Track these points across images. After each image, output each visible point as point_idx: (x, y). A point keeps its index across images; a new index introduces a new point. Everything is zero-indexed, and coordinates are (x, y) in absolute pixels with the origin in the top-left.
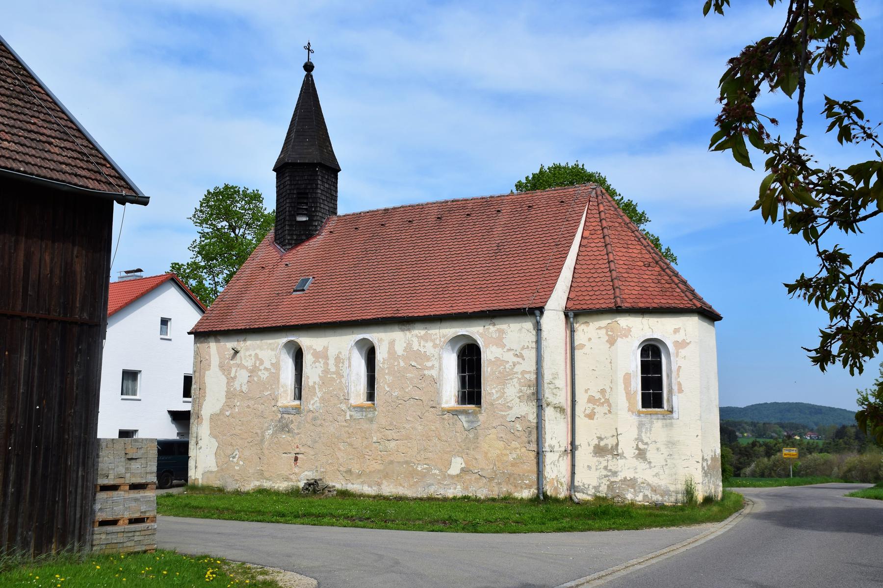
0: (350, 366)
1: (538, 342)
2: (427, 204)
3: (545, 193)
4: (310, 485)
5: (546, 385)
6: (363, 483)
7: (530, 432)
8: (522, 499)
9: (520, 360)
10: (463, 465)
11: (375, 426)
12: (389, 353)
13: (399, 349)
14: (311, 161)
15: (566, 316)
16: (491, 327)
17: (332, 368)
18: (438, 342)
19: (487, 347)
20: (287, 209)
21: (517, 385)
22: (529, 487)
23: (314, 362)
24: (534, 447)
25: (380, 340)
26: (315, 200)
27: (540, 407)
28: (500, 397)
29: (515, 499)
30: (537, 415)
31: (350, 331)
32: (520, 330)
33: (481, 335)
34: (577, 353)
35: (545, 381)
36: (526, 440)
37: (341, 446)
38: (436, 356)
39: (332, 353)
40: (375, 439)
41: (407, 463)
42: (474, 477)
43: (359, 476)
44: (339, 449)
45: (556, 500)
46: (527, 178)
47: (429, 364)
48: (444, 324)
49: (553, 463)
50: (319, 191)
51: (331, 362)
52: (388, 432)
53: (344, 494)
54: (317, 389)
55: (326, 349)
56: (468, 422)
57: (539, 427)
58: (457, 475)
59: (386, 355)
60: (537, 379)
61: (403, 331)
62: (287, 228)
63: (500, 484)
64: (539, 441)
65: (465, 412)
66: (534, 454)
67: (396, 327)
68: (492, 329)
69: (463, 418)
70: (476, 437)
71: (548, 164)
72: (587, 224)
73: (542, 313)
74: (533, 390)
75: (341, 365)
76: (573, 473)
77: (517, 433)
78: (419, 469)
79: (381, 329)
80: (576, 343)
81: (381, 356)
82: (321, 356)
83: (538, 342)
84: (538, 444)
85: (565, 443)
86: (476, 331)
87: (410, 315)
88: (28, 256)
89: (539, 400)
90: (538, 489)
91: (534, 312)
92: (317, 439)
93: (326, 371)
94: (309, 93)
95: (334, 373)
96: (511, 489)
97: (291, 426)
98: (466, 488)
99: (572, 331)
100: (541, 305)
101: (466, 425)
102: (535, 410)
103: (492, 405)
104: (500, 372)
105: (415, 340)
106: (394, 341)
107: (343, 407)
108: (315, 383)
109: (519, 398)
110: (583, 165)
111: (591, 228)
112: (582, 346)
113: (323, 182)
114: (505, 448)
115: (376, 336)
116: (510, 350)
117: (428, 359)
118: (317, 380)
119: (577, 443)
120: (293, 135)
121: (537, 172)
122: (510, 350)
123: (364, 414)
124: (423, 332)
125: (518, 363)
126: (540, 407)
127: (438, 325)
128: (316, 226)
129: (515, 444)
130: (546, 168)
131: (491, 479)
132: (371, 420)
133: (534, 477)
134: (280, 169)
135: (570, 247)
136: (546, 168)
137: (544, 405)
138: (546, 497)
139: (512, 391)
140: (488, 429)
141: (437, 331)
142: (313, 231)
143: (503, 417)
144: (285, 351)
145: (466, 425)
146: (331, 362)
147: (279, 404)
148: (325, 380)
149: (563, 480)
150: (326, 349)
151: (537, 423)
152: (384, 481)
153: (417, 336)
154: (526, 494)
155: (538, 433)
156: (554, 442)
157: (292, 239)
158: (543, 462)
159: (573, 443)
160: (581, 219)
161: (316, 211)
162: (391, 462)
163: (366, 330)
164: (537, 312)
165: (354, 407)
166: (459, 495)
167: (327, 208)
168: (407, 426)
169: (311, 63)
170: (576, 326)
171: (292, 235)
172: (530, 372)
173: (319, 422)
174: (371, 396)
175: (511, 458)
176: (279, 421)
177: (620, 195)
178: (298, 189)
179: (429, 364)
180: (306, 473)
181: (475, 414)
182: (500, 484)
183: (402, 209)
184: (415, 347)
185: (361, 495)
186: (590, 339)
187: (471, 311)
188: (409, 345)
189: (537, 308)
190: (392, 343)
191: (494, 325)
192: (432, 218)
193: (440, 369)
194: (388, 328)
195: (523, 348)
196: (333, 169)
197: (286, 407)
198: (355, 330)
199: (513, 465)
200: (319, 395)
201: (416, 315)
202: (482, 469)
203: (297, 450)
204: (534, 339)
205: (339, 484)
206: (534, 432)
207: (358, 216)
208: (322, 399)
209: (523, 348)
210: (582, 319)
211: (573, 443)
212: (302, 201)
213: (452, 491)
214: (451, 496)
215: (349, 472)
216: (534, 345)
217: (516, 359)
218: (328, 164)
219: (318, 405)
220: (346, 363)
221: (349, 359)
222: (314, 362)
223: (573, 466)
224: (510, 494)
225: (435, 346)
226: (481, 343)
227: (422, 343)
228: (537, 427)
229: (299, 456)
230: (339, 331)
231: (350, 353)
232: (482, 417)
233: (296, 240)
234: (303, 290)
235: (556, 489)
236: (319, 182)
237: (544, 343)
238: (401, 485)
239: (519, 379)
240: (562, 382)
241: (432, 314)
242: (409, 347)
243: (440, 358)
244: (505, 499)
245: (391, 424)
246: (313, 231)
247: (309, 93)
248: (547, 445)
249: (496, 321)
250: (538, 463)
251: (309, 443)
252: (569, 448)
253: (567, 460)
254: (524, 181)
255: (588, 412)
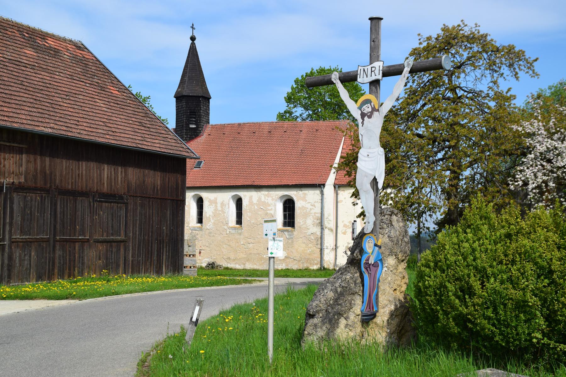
0: (229, 208)
1: (322, 200)
2: (262, 123)
3: (324, 123)
4: (210, 265)
5: (325, 219)
6: (236, 264)
7: (318, 240)
8: (313, 270)
9: (313, 207)
10: (286, 255)
11: (242, 237)
12: (249, 202)
13: (255, 200)
14: (197, 95)
15: (335, 187)
16: (300, 192)
17: (219, 208)
18: (274, 198)
19: (298, 201)
20: (185, 121)
21: (312, 219)
22: (317, 264)
23: (210, 205)
24: (319, 246)
25: (245, 196)
26: (200, 116)
27: (322, 229)
28: (304, 224)
29: (310, 269)
30: (321, 232)
31: (229, 190)
32: (314, 194)
33: (295, 195)
34: (339, 204)
35: (325, 217)
36: (316, 243)
37: (225, 246)
38: (273, 204)
39: (219, 201)
40: (242, 243)
41: (258, 254)
42: (291, 260)
43: (234, 260)
44: (224, 248)
45: (329, 270)
46: (302, 76)
47: (270, 208)
48: (277, 189)
49: (327, 254)
50: (202, 111)
51: (219, 205)
52: (249, 240)
53: (227, 268)
54: (211, 219)
55: (216, 199)
56: (289, 235)
57: (322, 238)
58: (283, 259)
59: (248, 203)
60: (321, 216)
61: (257, 191)
62: (185, 131)
63: (303, 263)
64: (321, 244)
65: (287, 231)
66: (320, 250)
67: (253, 190)
68: (300, 192)
69: (286, 233)
70: (292, 242)
71: (316, 68)
72: (345, 142)
73: (324, 187)
74: (319, 221)
75: (224, 207)
76: (336, 259)
77: (312, 241)
78: (265, 257)
79: (245, 190)
80: (339, 200)
81: (245, 203)
82: (213, 202)
83: (322, 200)
84: (321, 245)
85: (333, 245)
86: (293, 194)
87: (261, 184)
88: (169, 178)
89: (322, 225)
90: (321, 265)
91: (321, 186)
92: (211, 243)
93: (216, 210)
94: (193, 53)
95: (220, 211)
96: (308, 265)
97: (197, 236)
98: (287, 265)
99: (337, 194)
100: (324, 183)
101: (288, 237)
102: (320, 230)
103: (300, 227)
104: (304, 213)
105: (263, 196)
106: (252, 196)
107: (226, 227)
108: (210, 215)
109: (313, 224)
110: (341, 69)
111: (347, 144)
112: (342, 201)
113: (203, 106)
114: (306, 247)
115: (242, 194)
116: (309, 203)
117: (269, 205)
118: (211, 214)
119: (338, 245)
120: (186, 78)
121: (309, 72)
122: (309, 203)
123: (237, 231)
124: (267, 193)
125: (313, 209)
126: (322, 229)
127: (274, 189)
128: (200, 131)
129: (310, 245)
130: (315, 70)
131: (299, 261)
132: (240, 234)
133: (319, 260)
134: (179, 97)
135: (337, 154)
136: (315, 70)
137: (324, 228)
138: (324, 269)
139: (310, 221)
140: (298, 238)
141: (274, 192)
142: (198, 133)
143: (305, 233)
144: (192, 199)
145: (288, 237)
146: (219, 205)
147: (190, 226)
148: (215, 215)
149: (331, 262)
150: (216, 199)
151: (321, 236)
152: (247, 263)
153: (264, 194)
154: (315, 267)
155: (321, 240)
156: (328, 245)
157: (187, 137)
158: (323, 253)
159: (336, 245)
160: (342, 139)
161: (200, 122)
162: (251, 254)
163: (237, 190)
164: (322, 186)
165: (231, 228)
166: (284, 268)
167: (205, 120)
168: (259, 237)
169: (194, 36)
170: (339, 192)
171: (187, 135)
172: (318, 213)
173: (212, 235)
174: (239, 221)
175: (308, 251)
176: (191, 234)
177: (363, 90)
178: (190, 110)
179: (270, 208)
180: (206, 259)
181: (292, 231)
182: (303, 263)
183: (248, 124)
184: (263, 199)
185: (235, 269)
186: (345, 198)
187: (291, 184)
188: (260, 199)
189: (322, 184)
190: (251, 197)
191: (302, 191)
192: (266, 131)
193: (275, 210)
194: (249, 190)
195: (315, 202)
196: (207, 98)
197: (194, 227)
198: (232, 190)
199: (309, 255)
200: (212, 221)
201: (263, 184)
202: (295, 257)
203: (201, 248)
204: (320, 198)
205: (225, 264)
206: (320, 240)
207: (223, 127)
208: (214, 224)
209: (315, 202)
210: (342, 189)
211: (336, 245)
212: (192, 116)
213: (280, 266)
214: (280, 269)
215: (229, 258)
216: (320, 201)
217: (312, 207)
218: (206, 96)
219: (212, 226)
220: (227, 206)
221: (228, 204)
222: (210, 205)
223: (336, 255)
224: (308, 267)
225: (273, 199)
226: (295, 199)
227: (266, 198)
228: (321, 238)
229: (202, 251)
230: (223, 190)
231: (229, 201)
232: (295, 233)
233: (189, 138)
234: (200, 168)
235: (328, 265)
236: (202, 106)
237: (325, 200)
238: (255, 264)
239: (313, 216)
240: (332, 218)
241: (272, 184)
242: (259, 200)
243: (275, 205)
244: (306, 269)
245: (250, 236)
246: (198, 133)
247: (193, 53)
248: (325, 246)
249: (302, 189)
250: (321, 254)
251: (207, 245)
252: (334, 247)
253: (334, 252)
254: (300, 78)
255: (343, 231)
